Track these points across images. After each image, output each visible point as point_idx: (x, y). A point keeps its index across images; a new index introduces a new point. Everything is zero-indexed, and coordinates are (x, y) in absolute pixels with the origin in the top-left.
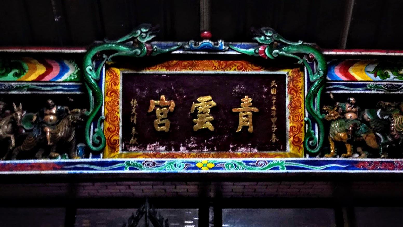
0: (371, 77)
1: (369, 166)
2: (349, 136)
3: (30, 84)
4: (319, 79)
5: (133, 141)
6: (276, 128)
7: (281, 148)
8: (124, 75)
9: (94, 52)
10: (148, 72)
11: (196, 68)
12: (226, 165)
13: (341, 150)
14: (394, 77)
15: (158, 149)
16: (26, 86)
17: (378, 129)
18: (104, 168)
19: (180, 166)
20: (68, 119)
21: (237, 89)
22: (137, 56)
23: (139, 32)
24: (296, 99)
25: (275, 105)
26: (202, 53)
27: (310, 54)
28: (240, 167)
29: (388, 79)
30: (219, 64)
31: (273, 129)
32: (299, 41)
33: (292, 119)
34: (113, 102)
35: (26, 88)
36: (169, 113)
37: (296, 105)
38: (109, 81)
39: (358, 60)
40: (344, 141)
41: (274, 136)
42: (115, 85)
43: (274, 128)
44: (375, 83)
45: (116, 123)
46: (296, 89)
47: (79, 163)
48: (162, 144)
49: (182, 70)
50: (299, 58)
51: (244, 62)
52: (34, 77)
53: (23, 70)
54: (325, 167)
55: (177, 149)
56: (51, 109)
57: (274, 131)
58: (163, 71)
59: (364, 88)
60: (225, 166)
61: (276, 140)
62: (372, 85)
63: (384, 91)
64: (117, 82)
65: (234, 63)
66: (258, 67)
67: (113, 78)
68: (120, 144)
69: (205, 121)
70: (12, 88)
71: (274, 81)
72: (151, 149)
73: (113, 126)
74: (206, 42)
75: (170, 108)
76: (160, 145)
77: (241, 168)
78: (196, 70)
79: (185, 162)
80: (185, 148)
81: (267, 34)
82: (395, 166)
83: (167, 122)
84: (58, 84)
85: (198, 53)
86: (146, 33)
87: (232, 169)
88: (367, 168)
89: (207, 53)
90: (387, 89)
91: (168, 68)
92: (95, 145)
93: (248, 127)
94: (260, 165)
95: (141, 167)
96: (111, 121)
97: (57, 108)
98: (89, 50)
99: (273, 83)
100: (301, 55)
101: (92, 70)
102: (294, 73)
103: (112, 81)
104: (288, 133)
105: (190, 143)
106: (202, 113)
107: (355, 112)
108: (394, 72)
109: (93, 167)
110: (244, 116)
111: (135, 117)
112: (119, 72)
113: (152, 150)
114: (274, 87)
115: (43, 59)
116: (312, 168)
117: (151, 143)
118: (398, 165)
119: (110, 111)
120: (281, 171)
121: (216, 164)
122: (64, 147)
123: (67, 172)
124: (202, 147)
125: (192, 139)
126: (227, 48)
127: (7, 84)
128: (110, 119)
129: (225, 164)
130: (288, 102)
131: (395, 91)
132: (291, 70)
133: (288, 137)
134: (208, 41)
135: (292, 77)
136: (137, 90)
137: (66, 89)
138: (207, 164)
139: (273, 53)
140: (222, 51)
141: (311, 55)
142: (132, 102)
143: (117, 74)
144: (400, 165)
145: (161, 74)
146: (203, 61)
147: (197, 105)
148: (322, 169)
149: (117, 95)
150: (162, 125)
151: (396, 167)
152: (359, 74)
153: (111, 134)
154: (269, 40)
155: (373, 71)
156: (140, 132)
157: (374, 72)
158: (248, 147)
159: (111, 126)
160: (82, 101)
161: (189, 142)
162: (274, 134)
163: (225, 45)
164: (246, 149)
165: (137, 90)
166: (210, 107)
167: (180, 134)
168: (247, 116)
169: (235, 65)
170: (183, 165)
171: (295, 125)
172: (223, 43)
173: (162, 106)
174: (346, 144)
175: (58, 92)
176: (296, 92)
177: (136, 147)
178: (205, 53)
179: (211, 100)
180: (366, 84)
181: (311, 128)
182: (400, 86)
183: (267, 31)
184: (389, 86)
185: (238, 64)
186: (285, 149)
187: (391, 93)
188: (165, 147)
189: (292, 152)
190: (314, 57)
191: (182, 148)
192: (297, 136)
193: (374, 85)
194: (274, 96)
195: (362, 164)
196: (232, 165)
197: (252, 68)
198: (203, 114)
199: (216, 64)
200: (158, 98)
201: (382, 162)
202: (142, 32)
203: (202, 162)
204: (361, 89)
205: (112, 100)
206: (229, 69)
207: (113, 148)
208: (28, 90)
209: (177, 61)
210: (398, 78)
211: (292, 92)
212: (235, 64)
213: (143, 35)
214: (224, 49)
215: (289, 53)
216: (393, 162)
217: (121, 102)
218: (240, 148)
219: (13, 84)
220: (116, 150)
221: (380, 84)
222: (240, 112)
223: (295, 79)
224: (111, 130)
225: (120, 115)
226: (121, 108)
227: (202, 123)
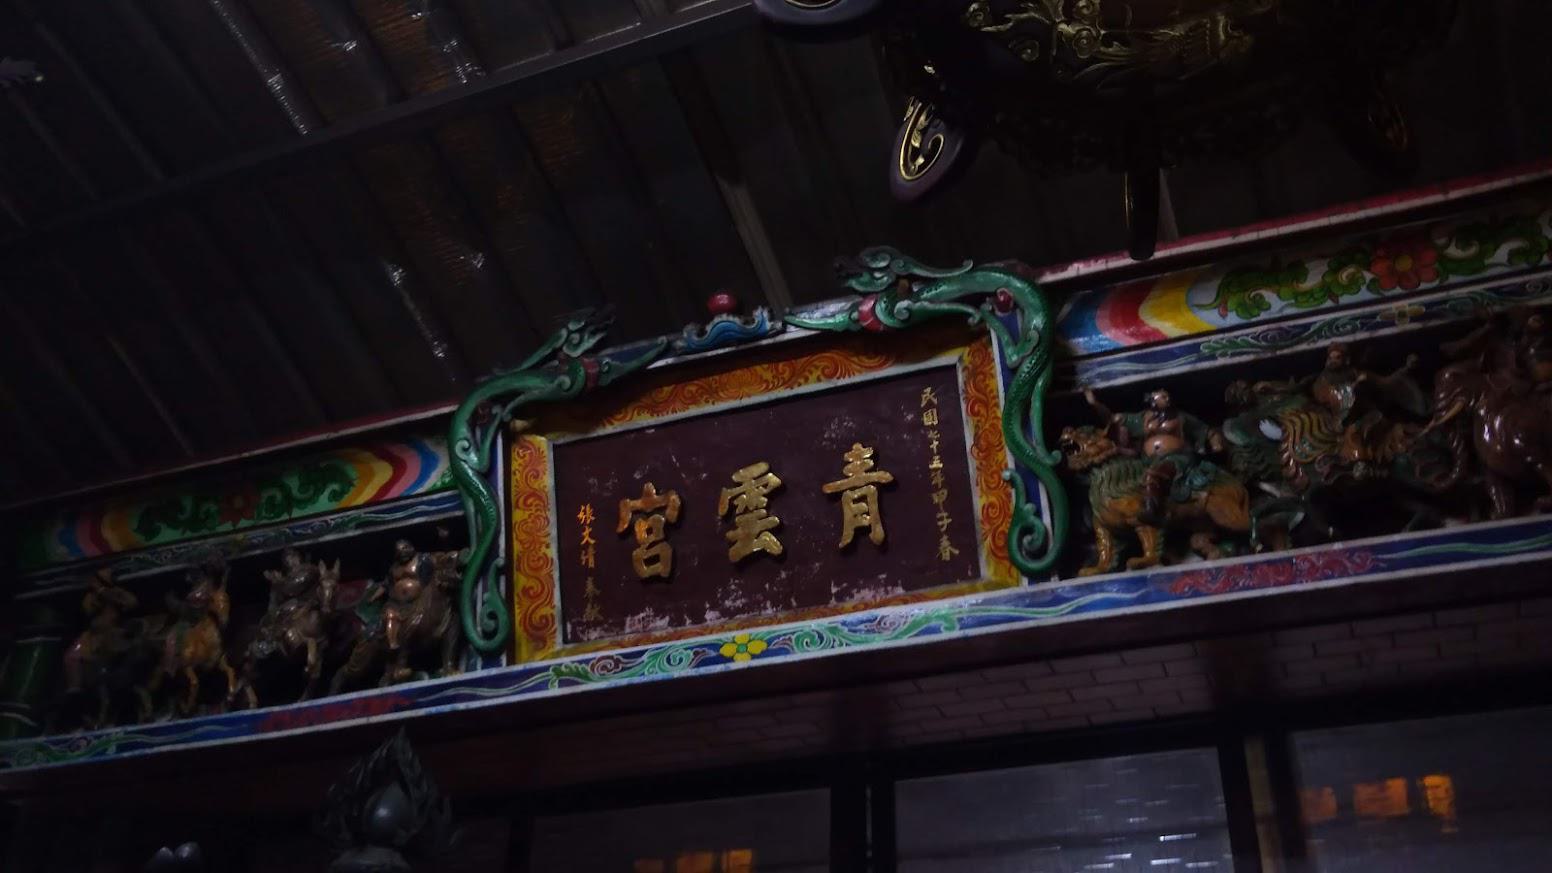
0: (1210, 319)
1: (1210, 582)
2: (1143, 504)
3: (361, 512)
4: (1029, 356)
5: (591, 613)
6: (948, 518)
7: (970, 573)
8: (556, 448)
9: (471, 405)
10: (609, 429)
11: (721, 394)
12: (798, 638)
13: (1128, 549)
14: (1284, 303)
15: (652, 625)
16: (355, 519)
17: (1262, 472)
18: (504, 691)
19: (681, 660)
21: (832, 431)
22: (565, 393)
23: (564, 333)
24: (987, 426)
25: (938, 454)
26: (721, 351)
27: (999, 291)
28: (834, 641)
29: (1263, 316)
30: (774, 372)
31: (940, 523)
32: (965, 263)
33: (984, 486)
34: (533, 522)
35: (353, 524)
36: (668, 526)
37: (989, 443)
38: (521, 469)
39: (1153, 277)
40: (1129, 521)
41: (945, 542)
42: (536, 477)
43: (942, 519)
44: (1227, 335)
45: (544, 572)
46: (983, 397)
47: (471, 688)
48: (660, 613)
49: (688, 408)
50: (970, 310)
51: (837, 354)
52: (368, 493)
53: (347, 484)
54: (1074, 606)
55: (698, 618)
56: (406, 563)
57: (944, 528)
58: (645, 420)
59: (1193, 357)
60: (793, 641)
61: (951, 554)
62: (1216, 342)
63: (1254, 353)
64: (539, 468)
65: (811, 362)
66: (877, 360)
67: (530, 461)
68: (558, 626)
69: (758, 531)
70: (327, 529)
71: (929, 390)
72: (634, 628)
73: (537, 582)
74: (724, 320)
75: (668, 512)
76: (655, 616)
77: (837, 642)
78: (721, 399)
79: (691, 648)
80: (717, 614)
81: (874, 266)
82: (1297, 570)
84: (419, 499)
85: (709, 354)
86: (580, 331)
87: (812, 648)
88: (1203, 589)
89: (733, 349)
90: (1263, 343)
91: (654, 410)
92: (488, 635)
93: (867, 529)
94: (888, 625)
95: (587, 678)
96: (532, 569)
97: (420, 559)
99: (928, 394)
100: (976, 299)
101: (469, 447)
103: (527, 470)
104: (978, 526)
105: (727, 598)
106: (746, 510)
107: (1171, 432)
108: (1284, 291)
109: (480, 691)
110: (856, 501)
111: (591, 551)
112: (541, 441)
113: (637, 632)
114: (930, 405)
115: (381, 445)
116: (1035, 613)
117: (633, 615)
118: (1306, 565)
119: (526, 546)
120: (945, 636)
121: (769, 642)
122: (426, 654)
123: (422, 712)
124: (758, 603)
125: (733, 587)
126: (779, 325)
127: (317, 522)
128: (528, 565)
129: (793, 637)
130: (969, 441)
131: (1291, 345)
132: (967, 349)
133: (979, 537)
134: (724, 317)
135: (970, 366)
136: (591, 481)
137: (433, 508)
138: (746, 645)
139: (895, 311)
140: (765, 336)
141: (1002, 293)
142: (581, 515)
143: (539, 449)
144: (1313, 565)
145: (642, 429)
146: (733, 373)
147: (731, 494)
148: (1067, 611)
149: (544, 502)
151: (1298, 573)
152: (1167, 322)
153: (533, 603)
154: (882, 277)
155: (1215, 300)
156: (604, 592)
157: (1218, 302)
158: (877, 585)
159: (532, 583)
161: (726, 595)
162: (945, 537)
163: (771, 320)
164: (872, 593)
165: (591, 481)
166: (765, 491)
168: (863, 499)
169: (817, 368)
170: (689, 655)
171: (993, 499)
172: (766, 314)
173: (649, 510)
174: (1139, 529)
175: (417, 520)
176: (986, 405)
177: (598, 629)
178: (727, 350)
179: (766, 473)
180: (1199, 344)
181: (1023, 499)
182: (1307, 327)
183: (875, 257)
184: (1271, 334)
185: (823, 360)
186: (977, 574)
187: (1279, 353)
188: (667, 618)
189: (993, 579)
190: (1011, 294)
191: (710, 615)
192: (1001, 529)
193: (1224, 341)
194: (934, 431)
195: (1188, 580)
196: (813, 637)
197: (862, 366)
198: (752, 512)
199: (768, 376)
201: (1252, 566)
202: (570, 332)
203: (736, 640)
204: (1182, 360)
205: (530, 516)
206: (802, 381)
207: (540, 640)
208: (358, 527)
209: (671, 388)
210: (1297, 304)
211: (976, 409)
212: (816, 363)
213: (576, 341)
214: (771, 330)
215: (941, 302)
216: (1289, 560)
217: (553, 517)
218: (858, 592)
219: (328, 518)
220: (549, 643)
221: (1242, 335)
222: (843, 491)
223: (979, 370)
224: (531, 592)
225: (552, 552)
226: (554, 532)
227: (748, 538)
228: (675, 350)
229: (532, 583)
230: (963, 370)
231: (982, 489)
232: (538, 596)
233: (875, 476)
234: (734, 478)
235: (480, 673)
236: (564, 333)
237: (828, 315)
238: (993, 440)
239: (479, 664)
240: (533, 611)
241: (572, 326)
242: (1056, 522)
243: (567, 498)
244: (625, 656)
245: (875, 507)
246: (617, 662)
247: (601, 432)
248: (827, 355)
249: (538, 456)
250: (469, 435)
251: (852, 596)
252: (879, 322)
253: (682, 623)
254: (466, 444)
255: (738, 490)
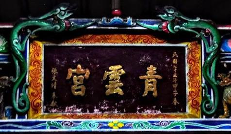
5: (53, 104)
8: (45, 47)
9: (19, 27)
10: (66, 44)
11: (108, 41)
18: (28, 127)
19: (94, 126)
24: (194, 68)
41: (175, 100)
42: (38, 55)
43: (175, 92)
45: (39, 88)
48: (78, 107)
50: (197, 33)
55: (92, 111)
57: (175, 96)
58: (79, 44)
61: (177, 103)
64: (40, 53)
68: (42, 106)
71: (175, 53)
72: (69, 111)
74: (117, 19)
75: (85, 75)
77: (147, 127)
81: (169, 12)
85: (109, 28)
86: (65, 11)
87: (139, 128)
89: (118, 28)
91: (83, 41)
92: (20, 107)
93: (152, 92)
96: (35, 86)
99: (175, 54)
100: (199, 30)
104: (187, 97)
106: (113, 80)
110: (149, 83)
111: (55, 83)
112: (41, 45)
113: (69, 112)
117: (69, 106)
121: (125, 124)
124: (113, 109)
126: (135, 24)
129: (133, 124)
130: (187, 71)
132: (190, 43)
133: (187, 100)
134: (118, 18)
136: (57, 60)
140: (130, 26)
142: (52, 71)
158: (152, 109)
159: (34, 91)
161: (102, 105)
164: (151, 111)
165: (57, 60)
166: (120, 75)
168: (152, 82)
169: (142, 39)
171: (193, 90)
172: (131, 20)
173: (79, 74)
176: (195, 62)
178: (115, 28)
179: (121, 69)
183: (169, 9)
185: (144, 37)
186: (184, 111)
188: (81, 109)
189: (191, 113)
191: (96, 110)
199: (125, 38)
202: (61, 10)
206: (136, 42)
207: (36, 110)
209: (91, 35)
211: (191, 62)
213: (62, 13)
217: (43, 70)
225: (42, 82)
226: (43, 75)
227: (113, 89)
228: (97, 24)
229: (34, 91)
230: (188, 49)
231: (190, 86)
232: (36, 96)
233: (157, 76)
234: (110, 68)
235: (17, 120)
236: (59, 10)
237: (144, 25)
238: (196, 72)
239: (17, 116)
240: (34, 101)
241: (63, 9)
242: (216, 101)
243: (49, 64)
244: (74, 122)
245: (155, 86)
246: (71, 124)
247: (63, 45)
248: (146, 36)
249: (39, 49)
250: (18, 38)
251: (144, 111)
252: (168, 29)
253: (85, 111)
254: (17, 41)
255: (110, 73)
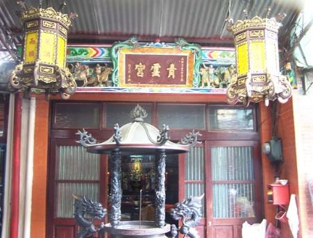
5: (129, 80)
20: (86, 73)
83: (142, 73)
98: (114, 46)
102: (138, 185)
150: (140, 74)
160: (111, 65)
167: (148, 78)
200: (138, 64)
